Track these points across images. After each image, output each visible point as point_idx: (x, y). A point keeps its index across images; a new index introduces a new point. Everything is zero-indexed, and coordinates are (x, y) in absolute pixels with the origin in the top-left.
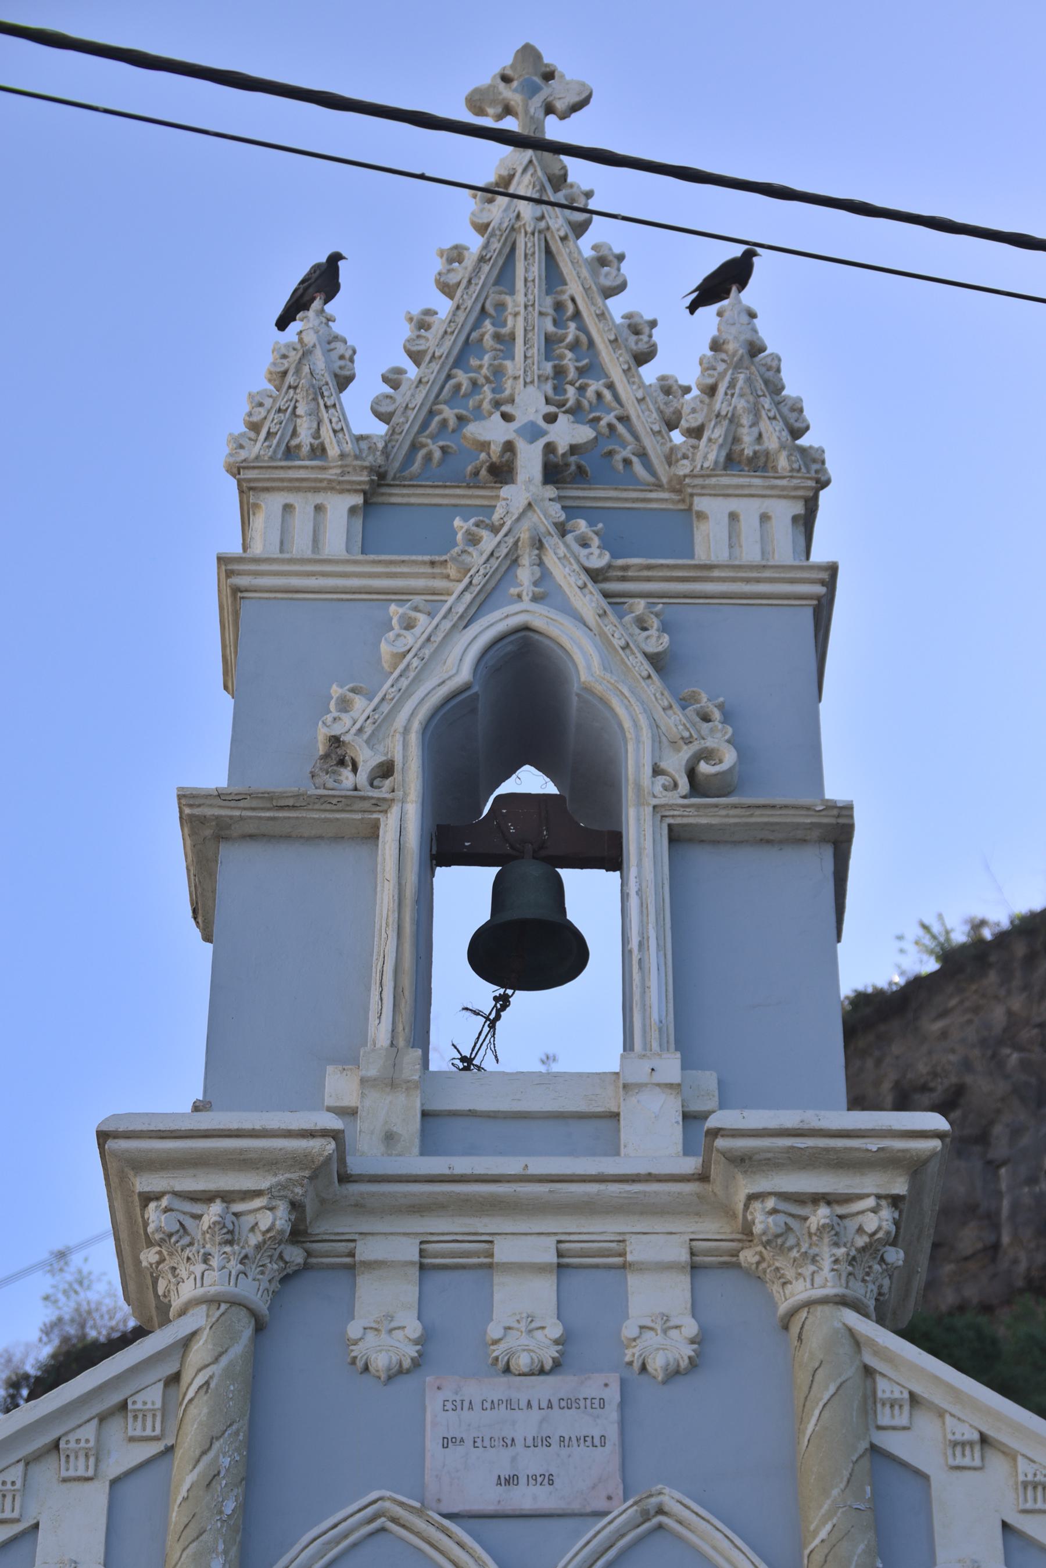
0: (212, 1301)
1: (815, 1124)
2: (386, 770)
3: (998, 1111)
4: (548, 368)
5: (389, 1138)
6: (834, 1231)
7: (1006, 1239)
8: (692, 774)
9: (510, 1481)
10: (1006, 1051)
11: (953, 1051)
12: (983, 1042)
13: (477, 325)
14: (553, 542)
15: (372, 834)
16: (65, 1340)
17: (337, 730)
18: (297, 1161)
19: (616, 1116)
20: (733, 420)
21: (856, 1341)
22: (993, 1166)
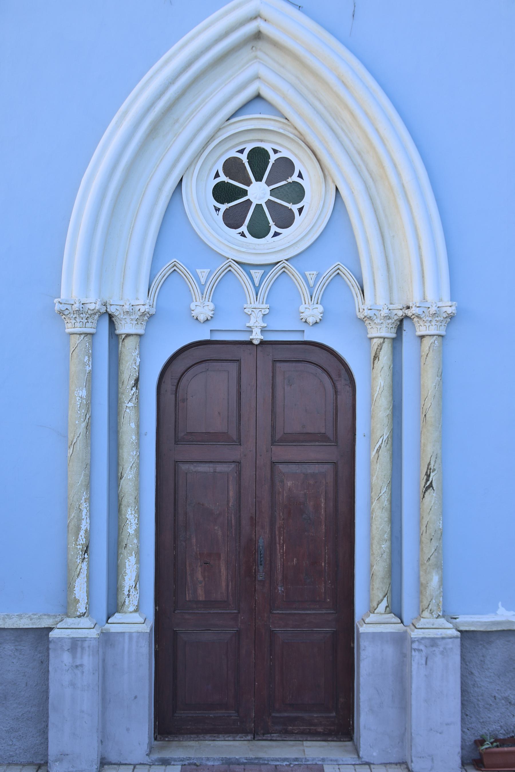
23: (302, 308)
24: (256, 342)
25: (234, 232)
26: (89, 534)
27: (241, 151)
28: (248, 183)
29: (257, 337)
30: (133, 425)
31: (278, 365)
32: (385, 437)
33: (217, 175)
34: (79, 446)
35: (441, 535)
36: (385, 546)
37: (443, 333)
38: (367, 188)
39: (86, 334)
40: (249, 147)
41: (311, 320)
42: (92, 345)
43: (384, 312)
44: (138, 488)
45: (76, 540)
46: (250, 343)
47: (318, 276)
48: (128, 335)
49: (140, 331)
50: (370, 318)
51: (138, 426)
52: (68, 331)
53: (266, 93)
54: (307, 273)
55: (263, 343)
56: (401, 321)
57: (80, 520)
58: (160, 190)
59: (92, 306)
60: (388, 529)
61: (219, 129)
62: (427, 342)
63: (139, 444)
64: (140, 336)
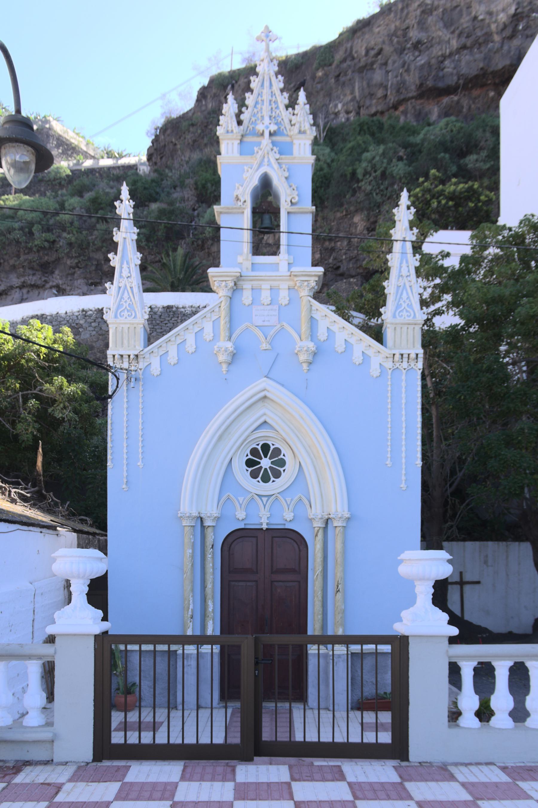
0: (225, 296)
1: (306, 270)
2: (245, 202)
3: (390, 56)
4: (270, 108)
5: (247, 269)
6: (308, 286)
7: (389, 93)
8: (291, 201)
9: (264, 321)
10: (394, 38)
11: (381, 37)
12: (388, 35)
13: (258, 97)
14: (270, 153)
15: (243, 213)
16: (167, 117)
17: (237, 194)
18: (234, 276)
19: (278, 264)
20: (300, 123)
21: (310, 302)
22: (387, 72)
23: (284, 514)
24: (264, 529)
25: (255, 481)
26: (193, 611)
27: (258, 445)
28: (261, 459)
29: (265, 527)
30: (211, 565)
31: (274, 539)
32: (320, 570)
33: (247, 455)
34: (189, 573)
35: (344, 611)
36: (320, 617)
37: (345, 525)
38: (313, 462)
39: (191, 526)
40: (261, 443)
41: (288, 520)
42: (194, 530)
43: (320, 516)
44: (213, 592)
45: (188, 613)
46: (262, 529)
47: (292, 500)
48: (209, 526)
49: (214, 524)
50: (314, 519)
51: (213, 565)
52: (183, 525)
53: (268, 421)
54: (287, 499)
55: (267, 529)
56: (327, 520)
57: (189, 604)
58: (222, 463)
59: (194, 515)
60: (321, 610)
61: (248, 436)
62: (338, 529)
63: (213, 573)
64: (214, 526)
